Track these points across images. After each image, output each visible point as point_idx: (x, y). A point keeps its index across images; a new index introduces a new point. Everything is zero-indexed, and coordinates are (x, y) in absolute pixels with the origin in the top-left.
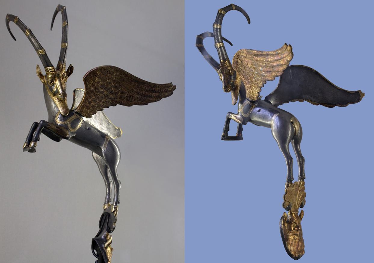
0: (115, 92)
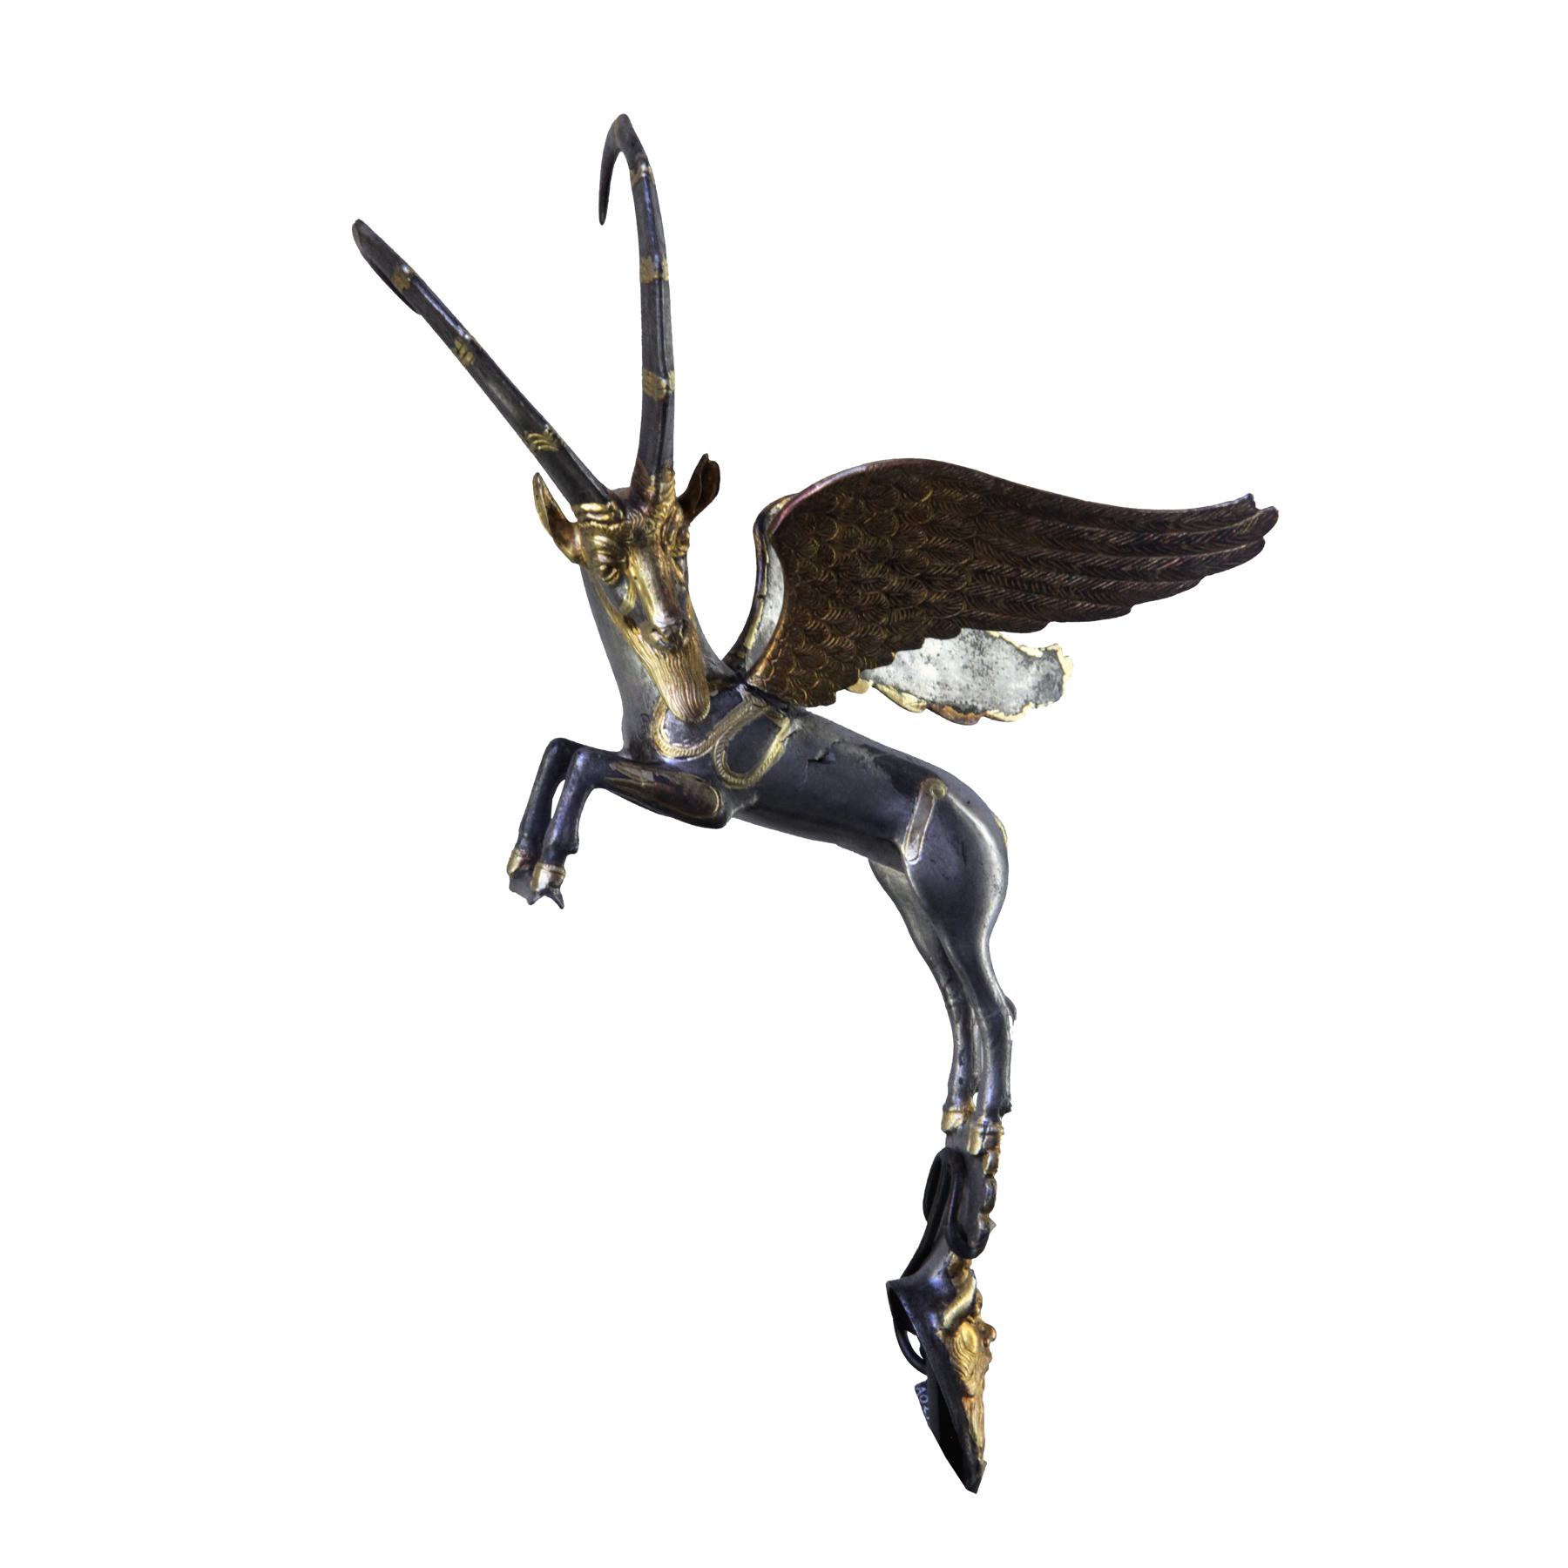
0: (944, 576)
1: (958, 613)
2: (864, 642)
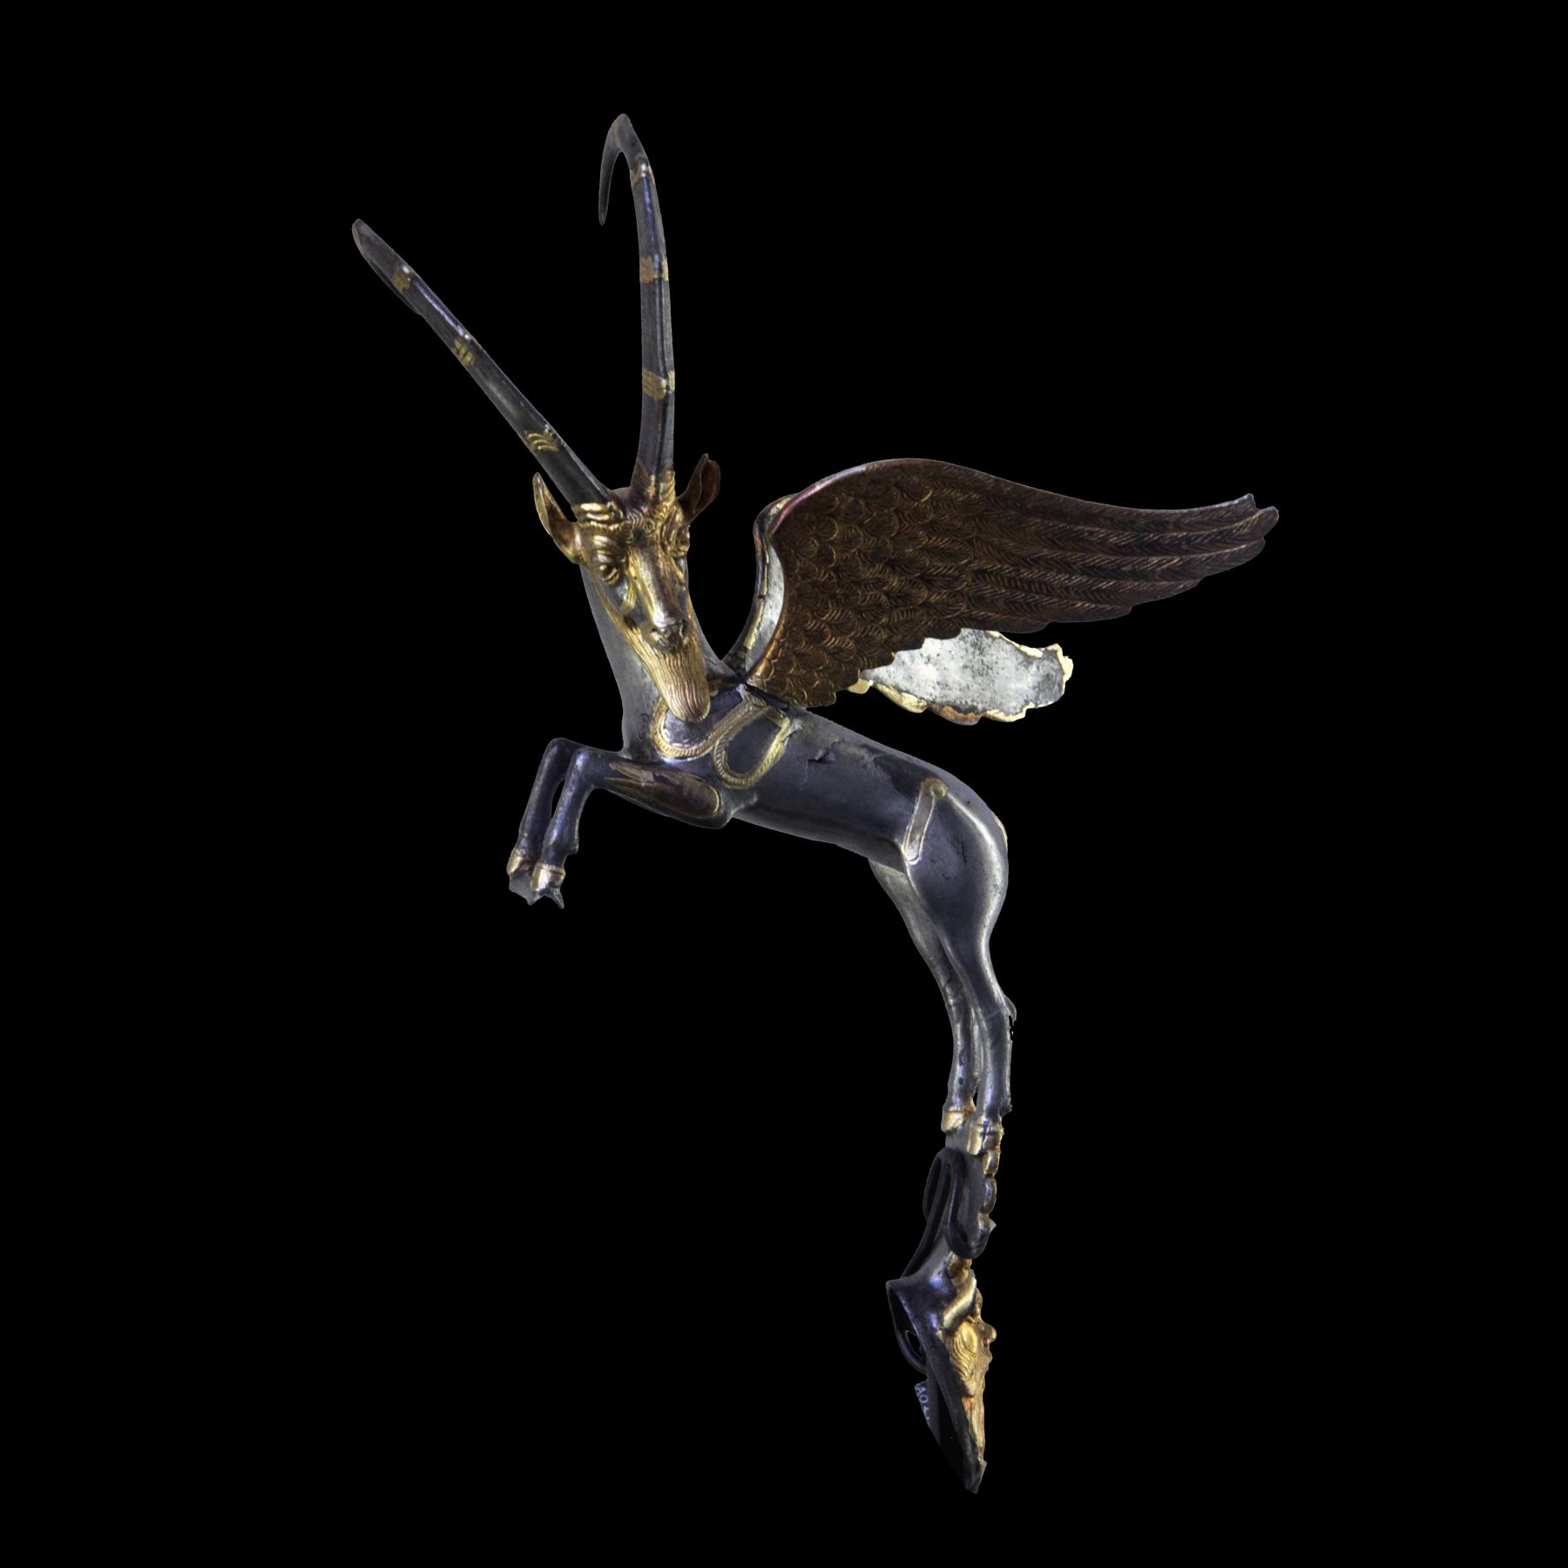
0: (944, 576)
1: (958, 613)
2: (864, 642)
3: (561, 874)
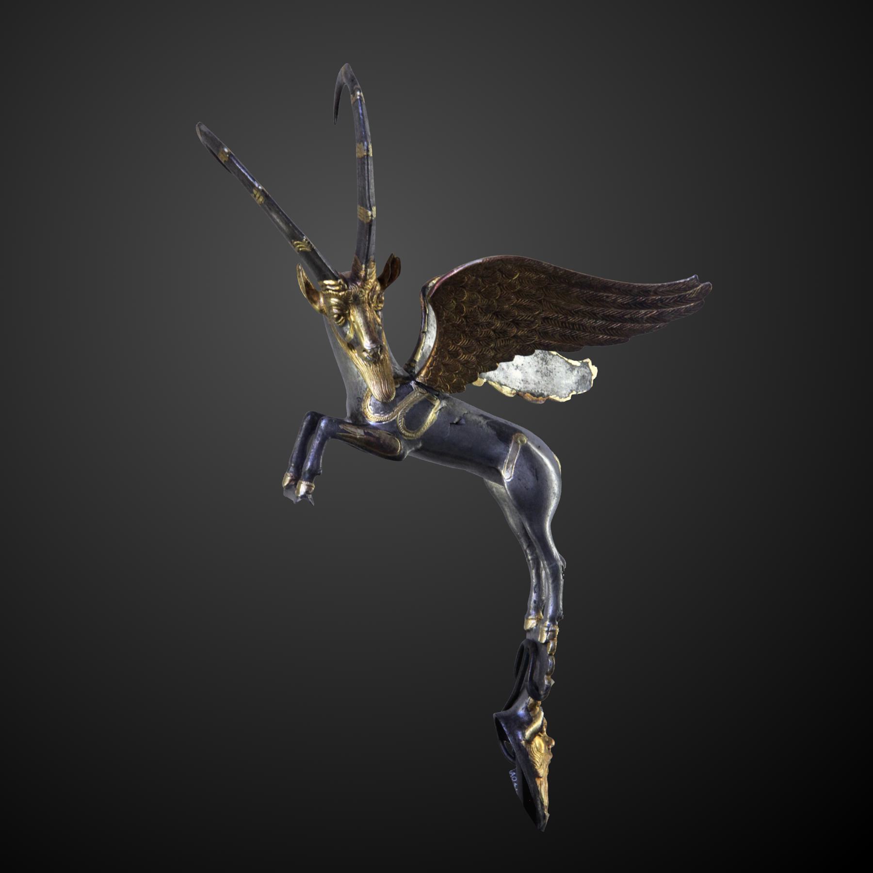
0: (525, 320)
1: (533, 341)
2: (481, 358)
3: (312, 487)
